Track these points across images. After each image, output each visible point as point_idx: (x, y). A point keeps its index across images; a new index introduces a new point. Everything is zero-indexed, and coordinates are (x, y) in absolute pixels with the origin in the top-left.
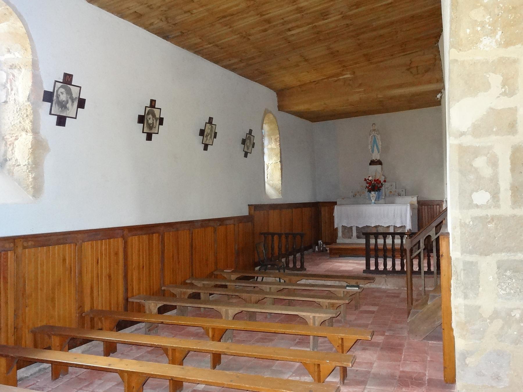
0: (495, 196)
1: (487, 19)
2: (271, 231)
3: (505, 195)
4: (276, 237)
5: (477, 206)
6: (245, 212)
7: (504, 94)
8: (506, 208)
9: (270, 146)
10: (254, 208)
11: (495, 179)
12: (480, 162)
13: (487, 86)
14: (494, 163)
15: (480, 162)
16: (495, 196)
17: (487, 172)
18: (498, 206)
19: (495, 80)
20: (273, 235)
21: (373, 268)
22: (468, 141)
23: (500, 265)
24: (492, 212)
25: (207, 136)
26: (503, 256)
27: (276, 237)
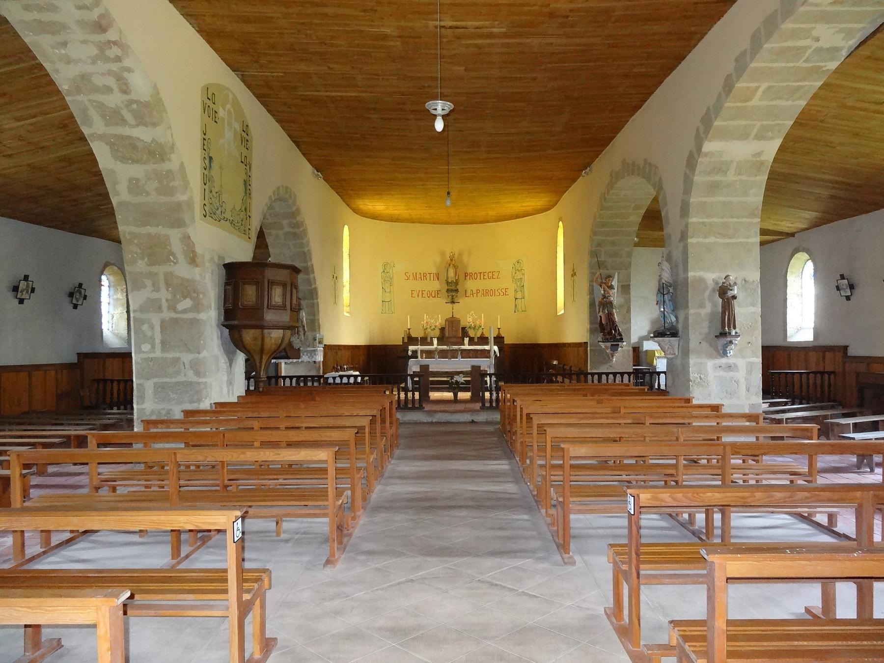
0: (153, 347)
1: (139, 251)
2: (109, 376)
3: (158, 346)
4: (115, 384)
5: (144, 352)
6: (74, 360)
7: (154, 291)
8: (158, 353)
9: (115, 297)
10: (81, 356)
11: (152, 338)
12: (145, 327)
13: (145, 287)
14: (152, 328)
15: (145, 327)
16: (153, 347)
17: (149, 333)
18: (154, 352)
19: (148, 282)
20: (112, 381)
21: (717, 517)
22: (138, 315)
23: (155, 384)
24: (152, 355)
25: (22, 292)
26: (156, 380)
27: (115, 384)
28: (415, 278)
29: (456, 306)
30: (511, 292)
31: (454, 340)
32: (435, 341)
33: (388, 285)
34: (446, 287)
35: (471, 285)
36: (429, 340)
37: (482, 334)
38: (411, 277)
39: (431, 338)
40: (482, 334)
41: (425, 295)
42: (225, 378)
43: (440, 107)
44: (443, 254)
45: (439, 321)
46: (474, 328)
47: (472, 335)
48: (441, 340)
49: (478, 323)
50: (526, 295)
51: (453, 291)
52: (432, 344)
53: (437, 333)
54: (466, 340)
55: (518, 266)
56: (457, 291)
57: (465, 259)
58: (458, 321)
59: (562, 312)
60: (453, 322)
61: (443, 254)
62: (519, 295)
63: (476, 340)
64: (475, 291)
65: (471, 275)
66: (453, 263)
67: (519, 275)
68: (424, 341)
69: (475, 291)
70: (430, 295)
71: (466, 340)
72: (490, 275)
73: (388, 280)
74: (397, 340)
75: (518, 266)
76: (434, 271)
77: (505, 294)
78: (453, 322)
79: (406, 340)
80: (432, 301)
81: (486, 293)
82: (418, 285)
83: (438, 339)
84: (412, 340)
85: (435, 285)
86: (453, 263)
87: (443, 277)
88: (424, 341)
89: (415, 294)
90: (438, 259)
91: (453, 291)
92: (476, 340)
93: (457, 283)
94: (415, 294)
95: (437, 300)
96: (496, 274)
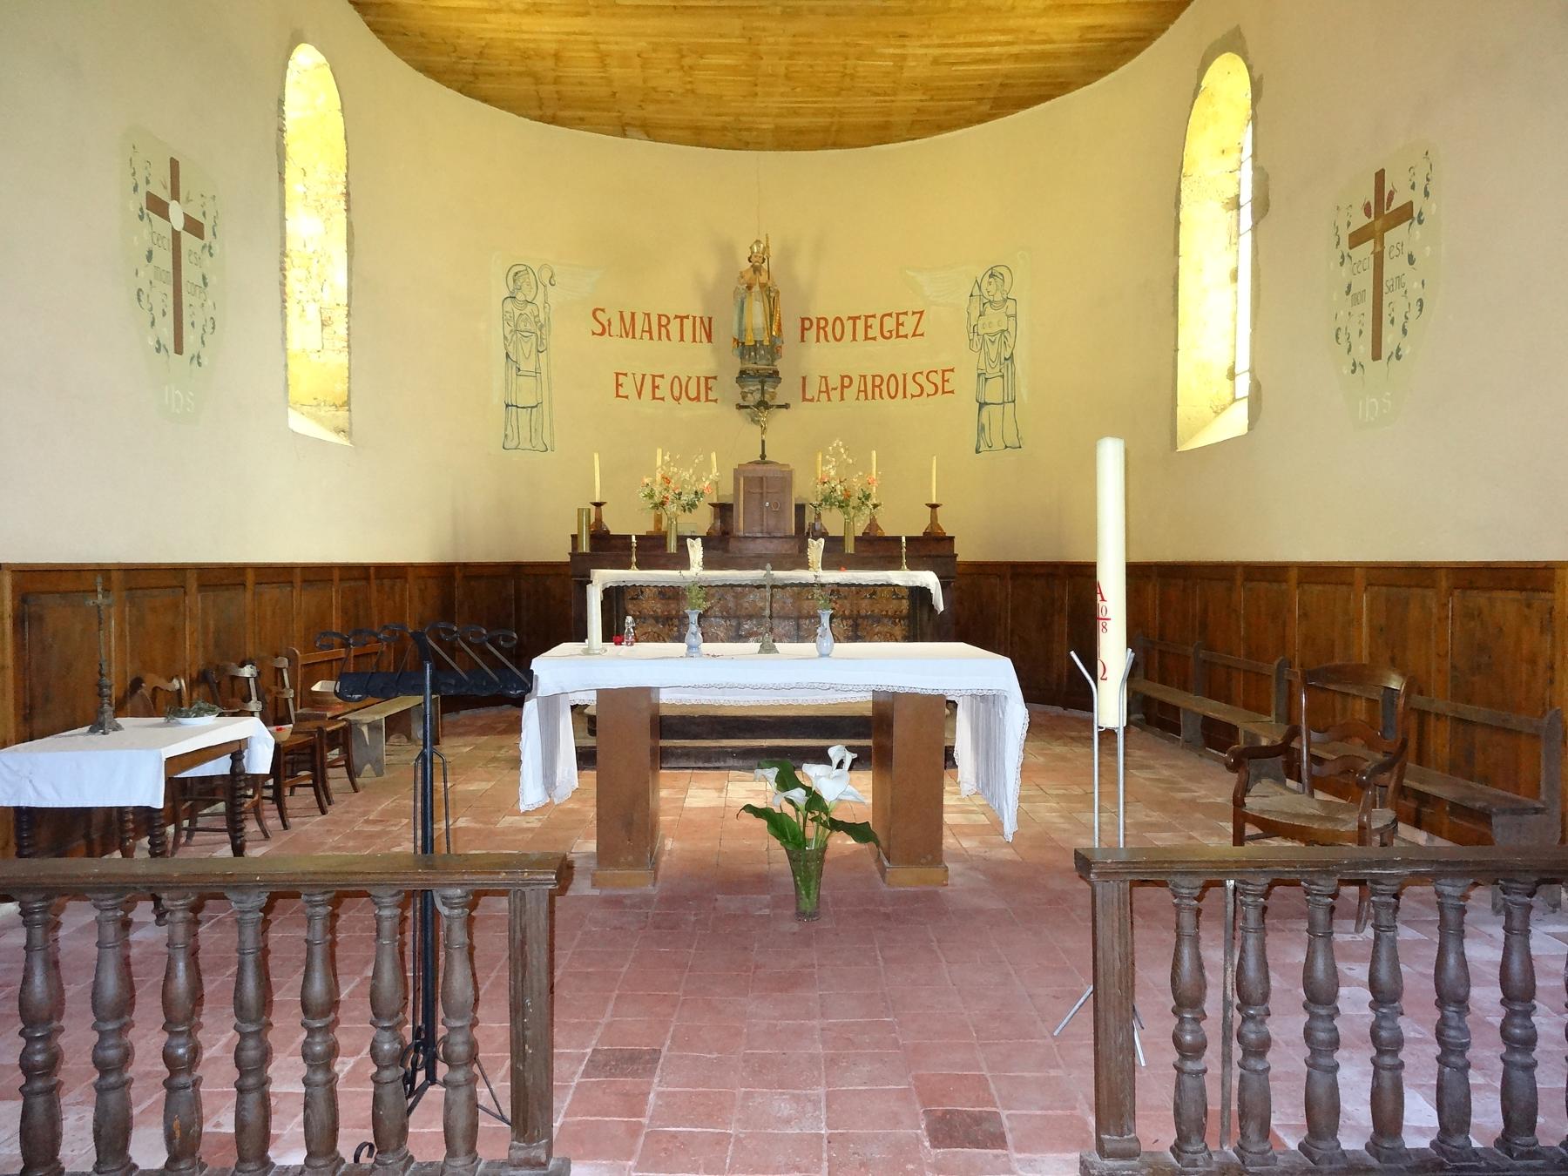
28: (629, 331)
29: (778, 419)
30: (964, 384)
31: (772, 547)
32: (696, 551)
33: (528, 346)
34: (736, 365)
35: (821, 359)
36: (672, 547)
37: (873, 524)
38: (616, 327)
39: (682, 540)
40: (873, 524)
41: (663, 391)
42: (1533, 817)
43: (247, 671)
44: (726, 251)
45: (713, 476)
46: (843, 505)
47: (835, 530)
48: (720, 546)
49: (856, 484)
50: (1023, 392)
51: (759, 377)
52: (682, 561)
53: (703, 520)
54: (816, 549)
55: (990, 288)
56: (775, 375)
57: (802, 268)
58: (785, 480)
59: (1235, 423)
60: (763, 481)
61: (726, 251)
62: (993, 392)
63: (850, 548)
64: (834, 381)
65: (821, 325)
66: (758, 279)
67: (995, 320)
68: (653, 549)
69: (834, 381)
70: (680, 391)
71: (816, 549)
72: (890, 324)
73: (526, 331)
74: (551, 543)
75: (990, 288)
76: (695, 309)
77: (942, 389)
78: (763, 481)
79: (585, 547)
80: (688, 411)
81: (876, 387)
82: (641, 355)
83: (707, 542)
84: (606, 546)
85: (699, 359)
86: (758, 279)
87: (726, 331)
88: (653, 549)
89: (628, 388)
90: (710, 269)
91: (759, 377)
92: (850, 548)
93: (774, 350)
94: (628, 388)
95: (703, 409)
96: (909, 323)
